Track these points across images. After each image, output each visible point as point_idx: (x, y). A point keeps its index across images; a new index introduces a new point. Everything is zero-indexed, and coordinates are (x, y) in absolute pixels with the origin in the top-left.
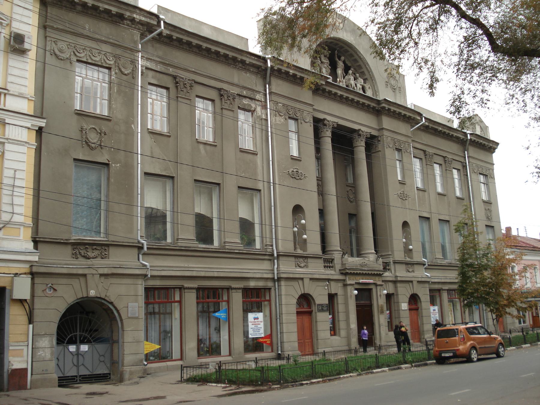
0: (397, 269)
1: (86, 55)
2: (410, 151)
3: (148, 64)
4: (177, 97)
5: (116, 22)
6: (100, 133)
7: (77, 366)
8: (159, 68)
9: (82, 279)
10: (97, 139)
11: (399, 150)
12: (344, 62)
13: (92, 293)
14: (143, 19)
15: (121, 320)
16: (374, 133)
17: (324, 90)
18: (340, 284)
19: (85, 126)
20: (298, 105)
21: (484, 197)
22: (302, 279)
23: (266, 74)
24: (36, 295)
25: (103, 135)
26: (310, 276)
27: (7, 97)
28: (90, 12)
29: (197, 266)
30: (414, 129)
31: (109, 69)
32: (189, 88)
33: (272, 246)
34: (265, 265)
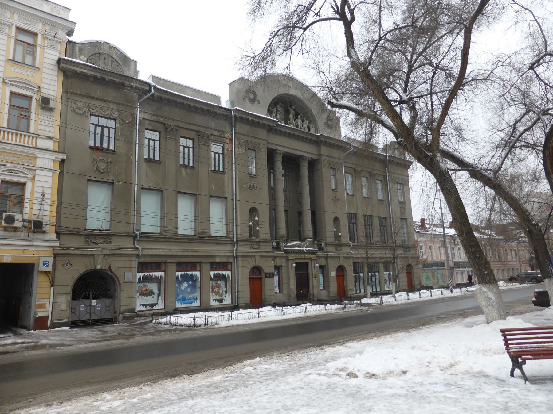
2: (342, 169)
3: (145, 116)
4: (199, 144)
7: (90, 313)
9: (91, 258)
10: (105, 166)
11: (334, 169)
12: (295, 110)
13: (98, 266)
14: (139, 86)
15: (120, 284)
16: (314, 157)
17: (276, 130)
18: (284, 260)
19: (96, 158)
20: (256, 141)
21: (401, 199)
22: (254, 256)
23: (232, 121)
24: (57, 268)
25: (109, 163)
26: (260, 254)
27: (38, 140)
30: (347, 154)
31: (115, 120)
32: (175, 131)
33: (233, 234)
34: (228, 248)
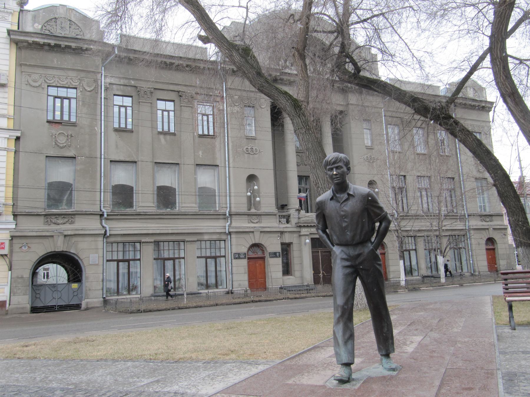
0: (233, 221)
1: (68, 82)
5: (79, 53)
6: (68, 136)
8: (122, 82)
9: (487, 231)
20: (478, 123)
25: (69, 137)
28: (56, 50)
29: (162, 226)
